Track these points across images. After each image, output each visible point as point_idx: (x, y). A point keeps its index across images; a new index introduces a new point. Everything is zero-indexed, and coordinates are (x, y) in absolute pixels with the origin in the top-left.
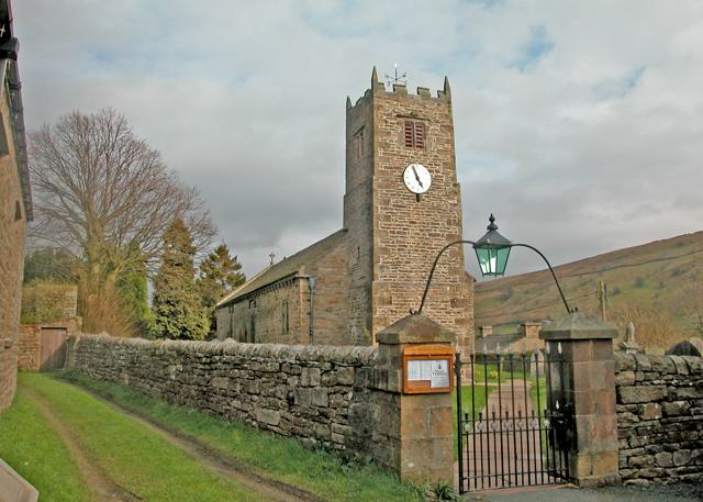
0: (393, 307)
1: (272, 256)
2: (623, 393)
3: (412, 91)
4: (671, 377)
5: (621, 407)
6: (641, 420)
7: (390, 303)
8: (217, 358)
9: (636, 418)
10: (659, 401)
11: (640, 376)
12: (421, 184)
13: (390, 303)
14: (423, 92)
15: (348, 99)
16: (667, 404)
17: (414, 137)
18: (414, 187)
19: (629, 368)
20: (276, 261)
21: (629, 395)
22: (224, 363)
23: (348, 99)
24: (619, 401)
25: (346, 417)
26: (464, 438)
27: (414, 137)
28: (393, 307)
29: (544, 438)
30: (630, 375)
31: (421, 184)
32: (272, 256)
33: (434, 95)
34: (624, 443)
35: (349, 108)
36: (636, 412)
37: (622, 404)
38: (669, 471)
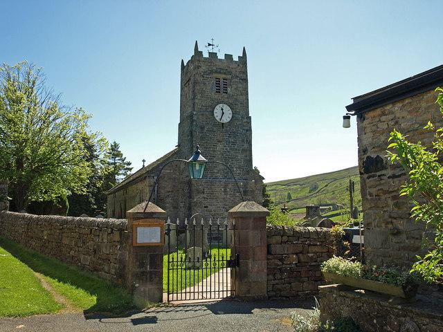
0: (205, 196)
1: (144, 161)
2: (273, 248)
3: (221, 56)
4: (305, 240)
5: (270, 257)
6: (283, 264)
7: (203, 193)
9: (280, 263)
10: (296, 254)
11: (285, 238)
12: (222, 109)
13: (203, 193)
14: (228, 57)
16: (301, 255)
17: (221, 87)
18: (227, 110)
19: (279, 234)
21: (277, 249)
23: (90, 314)
24: (269, 253)
27: (221, 87)
28: (205, 196)
29: (229, 275)
31: (222, 109)
32: (144, 161)
33: (236, 59)
34: (271, 277)
36: (281, 260)
38: (300, 293)
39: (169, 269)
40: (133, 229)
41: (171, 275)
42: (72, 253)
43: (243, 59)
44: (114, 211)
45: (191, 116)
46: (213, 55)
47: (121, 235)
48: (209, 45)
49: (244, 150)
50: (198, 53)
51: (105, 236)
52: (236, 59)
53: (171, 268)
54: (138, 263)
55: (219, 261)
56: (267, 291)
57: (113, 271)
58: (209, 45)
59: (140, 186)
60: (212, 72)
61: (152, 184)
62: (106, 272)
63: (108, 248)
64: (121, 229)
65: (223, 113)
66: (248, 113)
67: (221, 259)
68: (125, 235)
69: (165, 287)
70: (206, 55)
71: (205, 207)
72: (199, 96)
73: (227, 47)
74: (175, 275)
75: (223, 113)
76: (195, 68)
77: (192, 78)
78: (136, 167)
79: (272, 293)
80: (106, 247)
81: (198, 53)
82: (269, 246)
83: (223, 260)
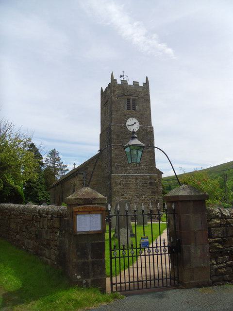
0: (122, 186)
1: (74, 164)
3: (130, 83)
7: (120, 184)
8: (12, 212)
12: (135, 123)
14: (136, 84)
15: (102, 89)
20: (76, 167)
22: (15, 215)
23: (102, 89)
25: (56, 246)
26: (113, 260)
28: (122, 186)
30: (218, 221)
31: (135, 123)
32: (74, 164)
33: (141, 85)
35: (102, 93)
37: (212, 238)
39: (111, 258)
40: (73, 215)
41: (113, 264)
42: (18, 236)
43: (147, 84)
44: (55, 200)
45: (109, 127)
46: (124, 83)
47: (60, 221)
48: (121, 76)
49: (149, 152)
50: (113, 81)
51: (46, 222)
52: (141, 85)
53: (113, 256)
54: (79, 253)
55: (161, 247)
56: (211, 276)
57: (54, 257)
58: (121, 76)
59: (73, 181)
60: (124, 95)
61: (82, 178)
62: (46, 257)
63: (49, 233)
64: (61, 216)
65: (133, 125)
66: (151, 125)
67: (162, 245)
68: (66, 222)
69: (108, 270)
70: (119, 82)
71: (122, 195)
72: (115, 113)
73: (134, 76)
74: (118, 264)
75: (133, 125)
76: (111, 93)
77: (109, 100)
78: (71, 168)
79: (215, 278)
80: (47, 233)
81: (113, 81)
82: (209, 229)
83: (165, 246)
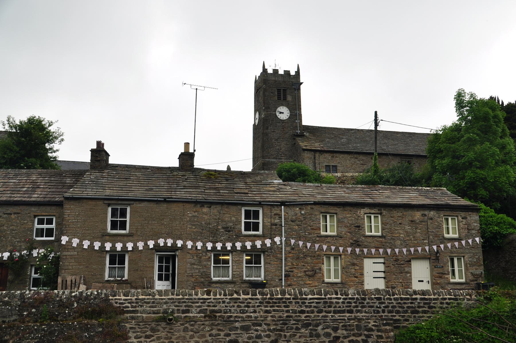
3: (281, 72)
14: (287, 73)
33: (293, 73)
43: (298, 73)
46: (276, 71)
50: (265, 70)
52: (293, 73)
